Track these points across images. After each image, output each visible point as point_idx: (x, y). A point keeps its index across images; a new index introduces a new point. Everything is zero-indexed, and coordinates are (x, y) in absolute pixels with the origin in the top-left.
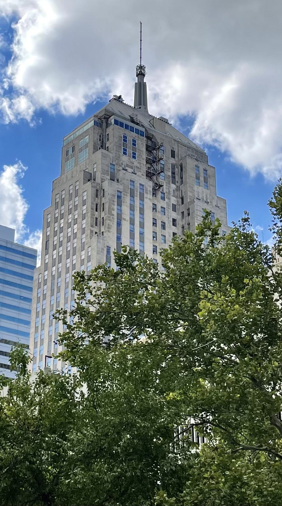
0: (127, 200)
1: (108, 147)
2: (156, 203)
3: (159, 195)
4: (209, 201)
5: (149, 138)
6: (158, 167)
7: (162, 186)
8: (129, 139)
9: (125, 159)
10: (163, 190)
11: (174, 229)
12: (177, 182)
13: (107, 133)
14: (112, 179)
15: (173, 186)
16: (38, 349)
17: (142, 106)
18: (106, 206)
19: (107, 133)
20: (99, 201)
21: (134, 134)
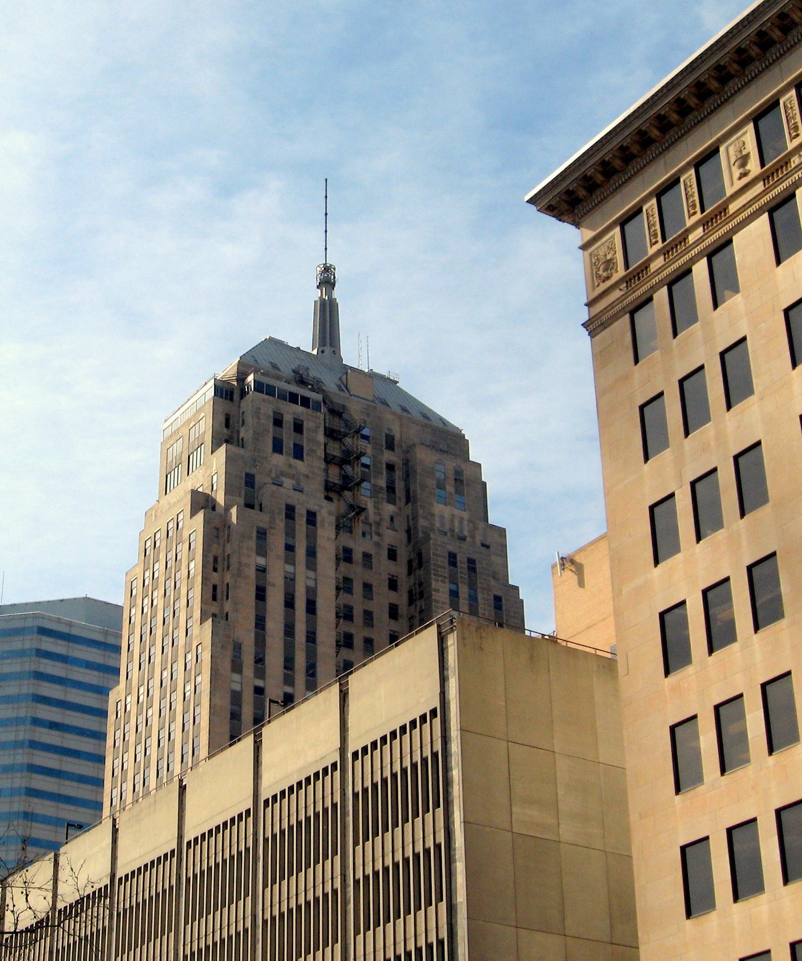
0: (277, 541)
1: (243, 439)
2: (351, 544)
3: (359, 528)
4: (466, 533)
5: (336, 412)
6: (354, 471)
7: (363, 510)
8: (288, 419)
9: (279, 460)
10: (367, 518)
11: (393, 597)
12: (400, 499)
13: (241, 411)
14: (249, 506)
15: (389, 509)
16: (359, 848)
17: (328, 349)
18: (234, 560)
19: (241, 411)
20: (220, 551)
21: (299, 409)
